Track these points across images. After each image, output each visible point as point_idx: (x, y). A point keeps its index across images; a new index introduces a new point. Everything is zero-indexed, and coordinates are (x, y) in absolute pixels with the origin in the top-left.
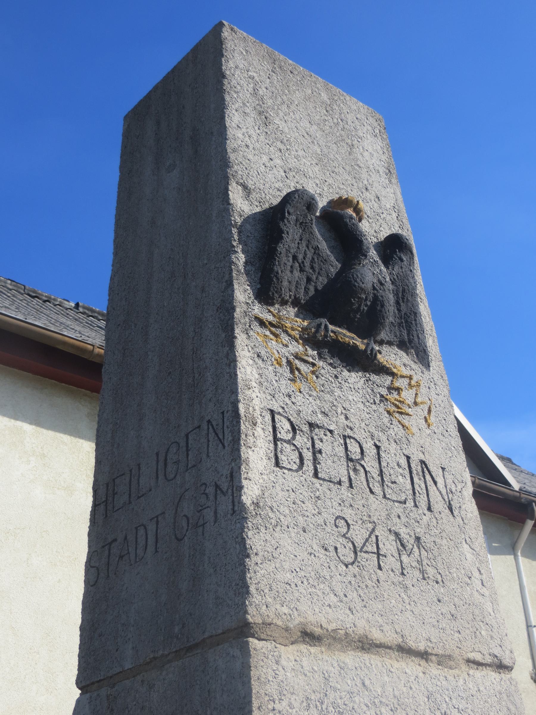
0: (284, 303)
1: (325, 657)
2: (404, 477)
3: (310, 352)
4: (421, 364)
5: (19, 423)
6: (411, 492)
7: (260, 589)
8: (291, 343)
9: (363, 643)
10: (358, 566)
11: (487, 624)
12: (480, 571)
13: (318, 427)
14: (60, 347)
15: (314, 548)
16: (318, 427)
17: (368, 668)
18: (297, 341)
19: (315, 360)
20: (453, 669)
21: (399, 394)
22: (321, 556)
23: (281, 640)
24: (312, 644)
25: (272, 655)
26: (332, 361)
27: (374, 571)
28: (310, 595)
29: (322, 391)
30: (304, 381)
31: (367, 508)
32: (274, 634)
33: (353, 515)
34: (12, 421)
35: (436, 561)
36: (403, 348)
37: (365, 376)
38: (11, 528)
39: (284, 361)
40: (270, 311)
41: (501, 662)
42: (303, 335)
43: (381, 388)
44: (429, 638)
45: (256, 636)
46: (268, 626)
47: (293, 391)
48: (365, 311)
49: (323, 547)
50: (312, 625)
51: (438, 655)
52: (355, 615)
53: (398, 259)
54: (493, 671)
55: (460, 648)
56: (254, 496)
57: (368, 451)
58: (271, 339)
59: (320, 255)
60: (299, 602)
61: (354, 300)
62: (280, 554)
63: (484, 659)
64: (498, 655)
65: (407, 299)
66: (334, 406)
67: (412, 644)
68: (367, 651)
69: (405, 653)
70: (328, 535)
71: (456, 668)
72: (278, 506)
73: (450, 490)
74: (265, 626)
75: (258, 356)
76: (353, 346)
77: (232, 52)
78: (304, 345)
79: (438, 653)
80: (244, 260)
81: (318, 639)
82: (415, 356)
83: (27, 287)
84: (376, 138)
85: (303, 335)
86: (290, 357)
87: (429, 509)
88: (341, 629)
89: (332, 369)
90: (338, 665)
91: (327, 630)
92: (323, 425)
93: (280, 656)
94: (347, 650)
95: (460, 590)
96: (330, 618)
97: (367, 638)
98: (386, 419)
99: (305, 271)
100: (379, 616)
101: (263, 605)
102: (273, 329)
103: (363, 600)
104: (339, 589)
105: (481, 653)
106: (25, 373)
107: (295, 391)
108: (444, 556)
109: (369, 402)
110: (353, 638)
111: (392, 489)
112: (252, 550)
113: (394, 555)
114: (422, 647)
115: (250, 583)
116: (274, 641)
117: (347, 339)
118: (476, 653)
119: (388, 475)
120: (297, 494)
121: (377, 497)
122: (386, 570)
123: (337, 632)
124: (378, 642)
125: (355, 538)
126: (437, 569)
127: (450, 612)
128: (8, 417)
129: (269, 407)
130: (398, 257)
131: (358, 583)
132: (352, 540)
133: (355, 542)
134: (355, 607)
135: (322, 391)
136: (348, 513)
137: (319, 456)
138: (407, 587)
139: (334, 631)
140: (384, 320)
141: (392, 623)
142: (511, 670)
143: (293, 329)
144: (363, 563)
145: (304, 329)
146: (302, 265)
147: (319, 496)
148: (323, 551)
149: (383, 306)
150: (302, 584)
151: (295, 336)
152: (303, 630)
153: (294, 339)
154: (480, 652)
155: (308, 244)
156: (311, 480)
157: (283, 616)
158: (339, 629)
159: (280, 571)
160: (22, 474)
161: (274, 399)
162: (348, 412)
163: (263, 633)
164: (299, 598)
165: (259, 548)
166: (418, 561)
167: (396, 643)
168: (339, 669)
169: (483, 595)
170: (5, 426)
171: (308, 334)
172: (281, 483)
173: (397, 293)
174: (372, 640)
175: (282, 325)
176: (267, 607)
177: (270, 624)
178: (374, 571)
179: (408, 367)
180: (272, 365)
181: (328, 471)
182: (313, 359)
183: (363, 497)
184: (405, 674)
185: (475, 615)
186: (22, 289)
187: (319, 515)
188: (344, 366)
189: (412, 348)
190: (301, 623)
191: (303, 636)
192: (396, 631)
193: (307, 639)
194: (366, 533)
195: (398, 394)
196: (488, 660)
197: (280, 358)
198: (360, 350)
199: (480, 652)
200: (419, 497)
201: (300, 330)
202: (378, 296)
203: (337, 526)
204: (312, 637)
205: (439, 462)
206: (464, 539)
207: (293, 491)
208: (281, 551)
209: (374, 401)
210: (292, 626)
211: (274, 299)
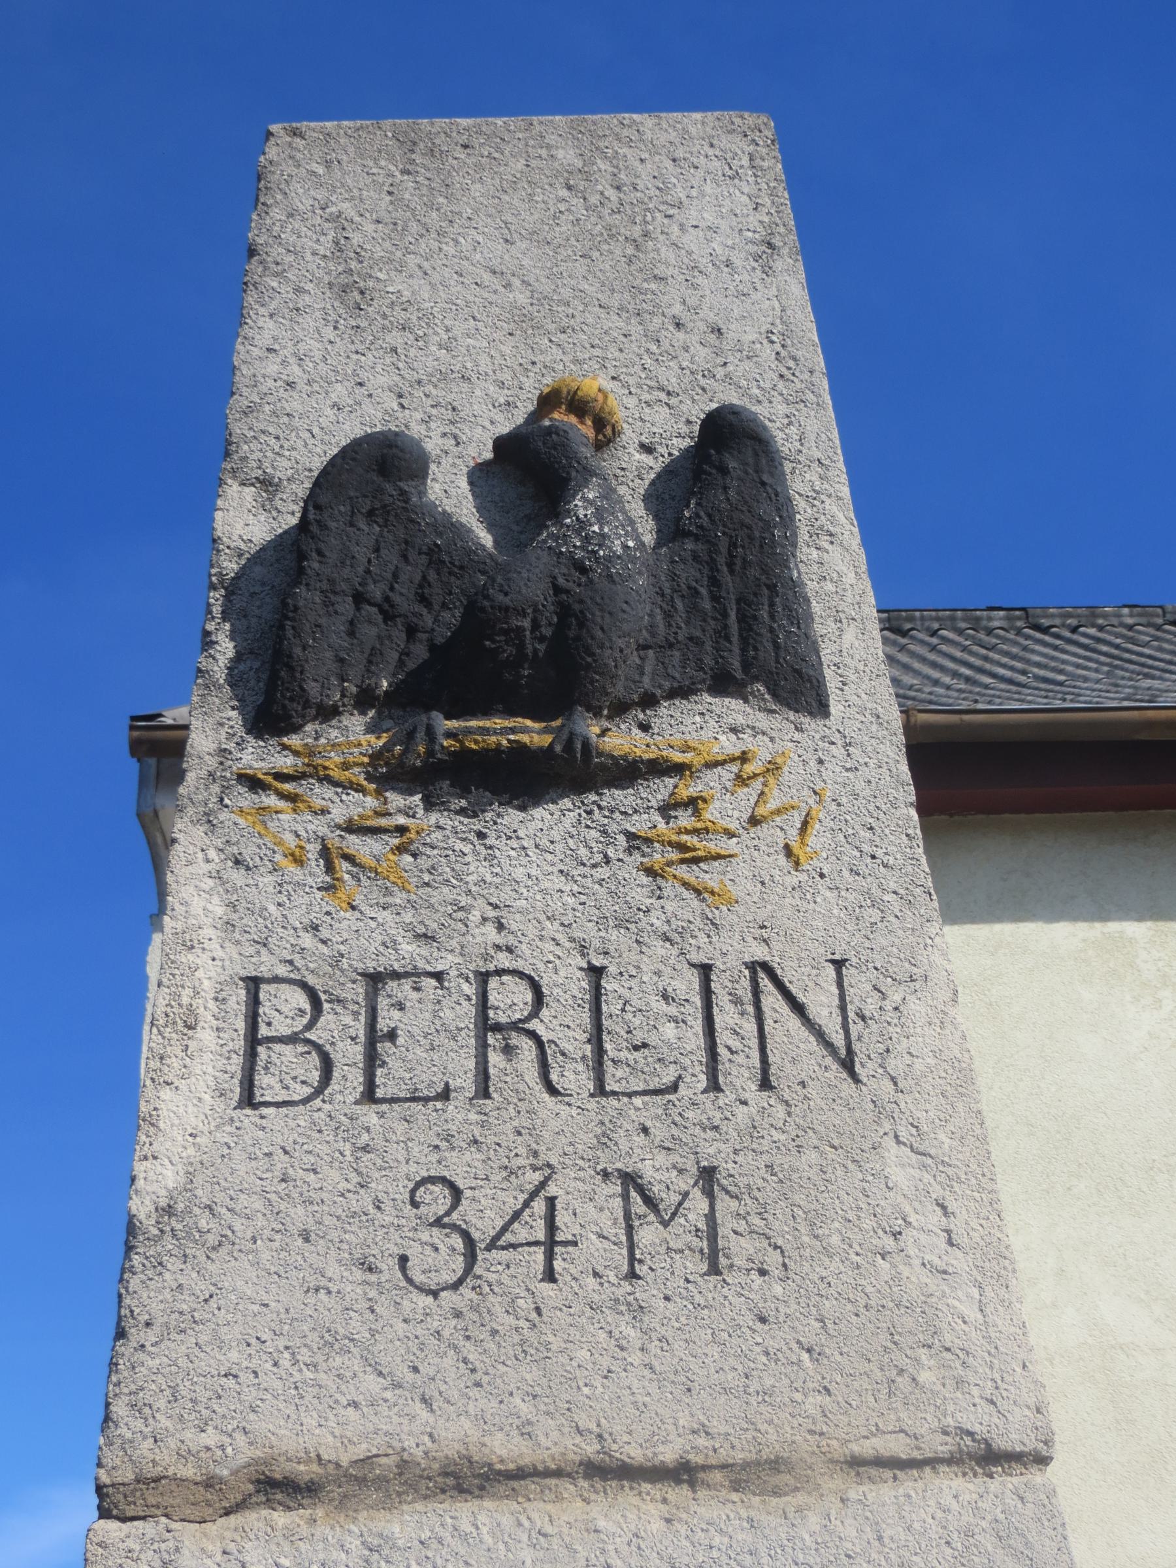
0: (328, 713)
1: (322, 1530)
2: (681, 1024)
3: (396, 800)
4: (790, 708)
5: (1113, 927)
6: (702, 1056)
7: (140, 1404)
8: (341, 801)
9: (457, 1477)
10: (474, 1288)
11: (948, 1350)
12: (944, 1208)
13: (396, 976)
14: (1143, 736)
15: (329, 1274)
16: (396, 976)
17: (464, 1537)
18: (360, 789)
19: (414, 817)
20: (786, 1494)
21: (697, 813)
22: (349, 1289)
23: (188, 1511)
24: (292, 1504)
25: (155, 1551)
26: (463, 803)
27: (528, 1290)
28: (296, 1388)
29: (427, 884)
30: (369, 878)
31: (530, 1135)
32: (168, 1500)
33: (479, 1164)
34: (1097, 925)
35: (766, 1216)
36: (730, 690)
37: (582, 802)
38: (1156, 1157)
39: (313, 849)
40: (285, 747)
41: (988, 1445)
42: (376, 769)
43: (636, 817)
44: (704, 1425)
45: (115, 1512)
46: (152, 1485)
47: (328, 913)
48: (541, 654)
49: (363, 1264)
50: (289, 1460)
51: (732, 1465)
52: (439, 1413)
53: (714, 471)
54: (964, 1474)
55: (822, 1434)
56: (163, 1193)
57: (556, 991)
58: (277, 812)
59: (444, 562)
60: (256, 1412)
61: (493, 641)
62: (219, 1309)
63: (918, 1448)
64: (977, 1428)
65: (744, 560)
66: (461, 909)
67: (634, 1453)
68: (477, 1492)
69: (612, 1479)
70: (381, 1232)
71: (797, 1489)
72: (232, 1199)
73: (857, 1014)
74: (144, 1487)
75: (237, 862)
76: (511, 749)
77: (283, 186)
78: (379, 793)
79: (731, 1461)
80: (231, 654)
81: (309, 1490)
82: (767, 696)
83: (1169, 608)
84: (736, 181)
85: (376, 769)
86: (330, 835)
87: (765, 1084)
88: (386, 1455)
89: (466, 821)
90: (363, 1543)
91: (338, 1465)
92: (415, 967)
93: (177, 1550)
94: (400, 1502)
95: (849, 1276)
96: (349, 1434)
97: (470, 1462)
98: (639, 891)
99: (400, 616)
100: (526, 1399)
101: (145, 1438)
102: (287, 787)
103: (473, 1371)
104: (394, 1359)
105: (907, 1434)
106: (1099, 814)
107: (333, 910)
108: (799, 1198)
109: (584, 865)
110: (424, 1470)
111: (629, 1065)
112: (134, 1319)
113: (605, 1234)
114: (668, 1455)
115: (116, 1395)
116: (166, 1516)
117: (494, 738)
118: (888, 1436)
119: (623, 1033)
120: (297, 1154)
121: (567, 1099)
122: (569, 1278)
123: (372, 1463)
124: (511, 1466)
125: (474, 1221)
126: (769, 1238)
127: (799, 1342)
128: (1085, 920)
129: (244, 973)
130: (715, 467)
131: (467, 1330)
132: (464, 1226)
133: (472, 1231)
134: (440, 1393)
135: (427, 884)
136: (458, 1166)
137: (383, 1047)
138: (641, 1307)
139: (367, 1460)
140: (592, 655)
141: (569, 1409)
142: (1048, 1464)
143: (346, 766)
144: (492, 1277)
145: (376, 757)
146: (386, 606)
147: (368, 1145)
148: (358, 1275)
149: (582, 624)
150: (275, 1370)
151: (351, 782)
152: (262, 1477)
153: (351, 788)
154: (902, 1431)
155: (406, 550)
156: (348, 1112)
157: (202, 1454)
158: (377, 1456)
159: (208, 1350)
160: (1149, 1033)
161: (263, 951)
162: (504, 913)
163: (135, 1504)
164: (259, 1402)
165: (156, 1308)
166: (697, 1230)
167: (577, 1458)
168: (367, 1553)
169: (945, 1272)
170: (1084, 940)
171: (387, 764)
172: (250, 1142)
173: (711, 557)
174: (490, 1465)
175: (315, 767)
176: (156, 1441)
177: (157, 1480)
178: (528, 1290)
179: (749, 731)
180: (275, 870)
181: (408, 1076)
182: (409, 816)
183: (519, 1112)
184: (595, 1535)
185: (900, 1334)
186: (1158, 616)
187: (362, 1191)
188: (503, 801)
189: (756, 679)
190: (255, 1462)
191: (266, 1490)
192: (577, 1427)
193: (279, 1496)
194: (515, 1198)
195: (693, 815)
196: (941, 1446)
197: (302, 848)
198: (535, 752)
199: (902, 1431)
200: (730, 1060)
201: (366, 760)
202: (569, 605)
203: (415, 1204)
204: (293, 1488)
205: (822, 950)
206: (892, 1135)
207: (286, 1152)
208: (221, 1302)
209: (606, 856)
210: (225, 1472)
211: (291, 717)
